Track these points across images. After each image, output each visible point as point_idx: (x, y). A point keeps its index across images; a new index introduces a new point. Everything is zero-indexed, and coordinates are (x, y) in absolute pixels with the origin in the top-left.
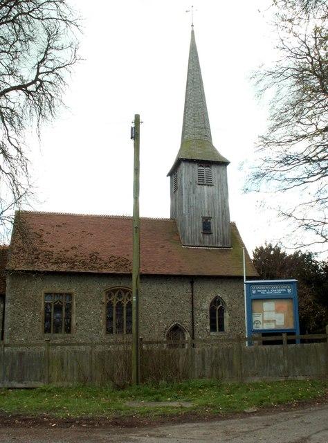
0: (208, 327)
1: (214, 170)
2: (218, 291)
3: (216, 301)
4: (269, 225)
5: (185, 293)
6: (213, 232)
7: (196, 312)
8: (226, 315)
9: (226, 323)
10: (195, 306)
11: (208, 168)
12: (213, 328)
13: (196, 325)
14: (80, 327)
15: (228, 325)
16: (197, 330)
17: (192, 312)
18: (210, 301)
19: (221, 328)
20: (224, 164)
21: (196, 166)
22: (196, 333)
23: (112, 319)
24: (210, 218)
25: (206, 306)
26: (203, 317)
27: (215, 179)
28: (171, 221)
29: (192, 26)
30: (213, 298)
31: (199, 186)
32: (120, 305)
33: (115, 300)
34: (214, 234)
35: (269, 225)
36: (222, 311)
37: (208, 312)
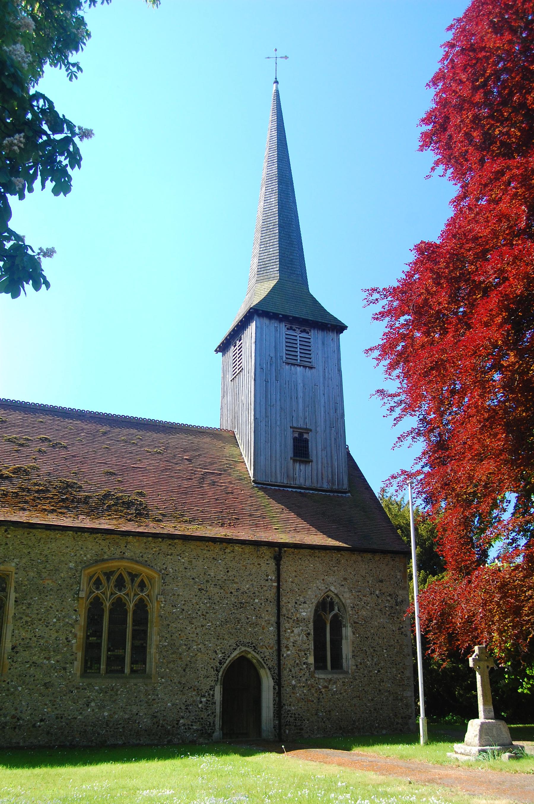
0: (311, 660)
1: (316, 338)
2: (331, 579)
3: (325, 605)
4: (384, 416)
5: (263, 583)
6: (314, 460)
7: (285, 625)
8: (348, 632)
9: (347, 649)
10: (284, 611)
11: (304, 335)
12: (320, 663)
13: (285, 653)
14: (24, 655)
15: (350, 655)
16: (287, 663)
17: (278, 623)
18: (315, 602)
19: (337, 663)
20: (339, 328)
21: (283, 328)
22: (285, 673)
23: (99, 646)
24: (308, 431)
25: (306, 612)
26: (299, 638)
27: (317, 355)
28: (59, 120)
29: (276, 50)
30: (320, 596)
31: (287, 367)
32: (119, 606)
33: (108, 595)
34: (314, 463)
35: (384, 416)
36: (337, 625)
37: (311, 625)
